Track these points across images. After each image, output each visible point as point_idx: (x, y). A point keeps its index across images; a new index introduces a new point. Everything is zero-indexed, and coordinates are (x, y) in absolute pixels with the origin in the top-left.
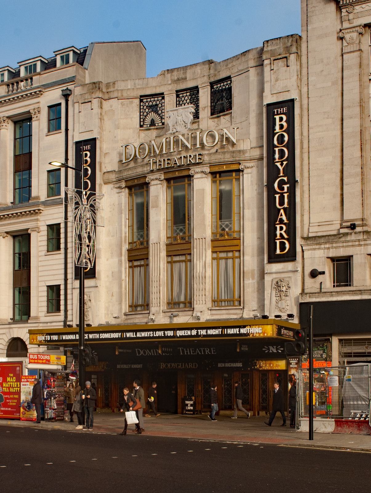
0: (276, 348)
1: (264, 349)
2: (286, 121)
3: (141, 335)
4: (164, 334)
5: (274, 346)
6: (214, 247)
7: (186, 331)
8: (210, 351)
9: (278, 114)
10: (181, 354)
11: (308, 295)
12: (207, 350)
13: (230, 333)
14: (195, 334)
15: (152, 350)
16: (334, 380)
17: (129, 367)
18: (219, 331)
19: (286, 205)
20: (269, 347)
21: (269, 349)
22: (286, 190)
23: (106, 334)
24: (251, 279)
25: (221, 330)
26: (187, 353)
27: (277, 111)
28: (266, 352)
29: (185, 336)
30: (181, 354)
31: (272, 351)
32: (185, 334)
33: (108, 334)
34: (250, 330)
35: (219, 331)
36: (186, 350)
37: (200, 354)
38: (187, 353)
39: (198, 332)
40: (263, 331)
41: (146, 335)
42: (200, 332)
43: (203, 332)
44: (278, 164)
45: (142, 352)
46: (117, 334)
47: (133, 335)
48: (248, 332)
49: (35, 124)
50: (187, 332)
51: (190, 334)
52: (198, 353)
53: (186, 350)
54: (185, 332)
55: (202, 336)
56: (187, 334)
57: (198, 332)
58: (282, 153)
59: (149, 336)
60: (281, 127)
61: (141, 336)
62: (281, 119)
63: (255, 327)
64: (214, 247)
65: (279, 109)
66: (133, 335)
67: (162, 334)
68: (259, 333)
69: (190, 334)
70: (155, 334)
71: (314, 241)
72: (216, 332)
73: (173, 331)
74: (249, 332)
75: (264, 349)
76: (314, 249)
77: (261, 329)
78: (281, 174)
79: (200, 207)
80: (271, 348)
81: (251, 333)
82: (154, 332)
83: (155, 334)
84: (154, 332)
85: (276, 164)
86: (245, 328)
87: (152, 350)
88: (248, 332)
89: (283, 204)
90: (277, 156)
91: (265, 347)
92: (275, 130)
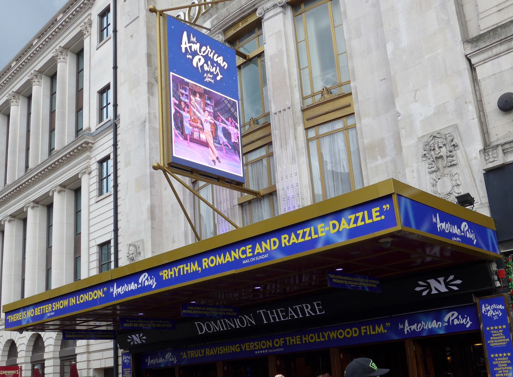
0: (445, 281)
1: (418, 289)
5: (439, 279)
6: (308, 120)
8: (313, 309)
10: (265, 322)
11: (500, 149)
12: (307, 308)
15: (218, 321)
16: (263, 206)
17: (201, 353)
20: (428, 281)
21: (429, 287)
24: (379, 157)
26: (274, 318)
28: (425, 293)
30: (265, 322)
31: (436, 289)
36: (272, 313)
37: (296, 317)
38: (274, 318)
42: (289, 340)
45: (205, 328)
49: (86, 42)
52: (292, 316)
53: (272, 313)
64: (308, 120)
71: (495, 38)
75: (418, 289)
76: (497, 56)
79: (277, 60)
80: (433, 283)
87: (218, 321)
91: (455, 288)
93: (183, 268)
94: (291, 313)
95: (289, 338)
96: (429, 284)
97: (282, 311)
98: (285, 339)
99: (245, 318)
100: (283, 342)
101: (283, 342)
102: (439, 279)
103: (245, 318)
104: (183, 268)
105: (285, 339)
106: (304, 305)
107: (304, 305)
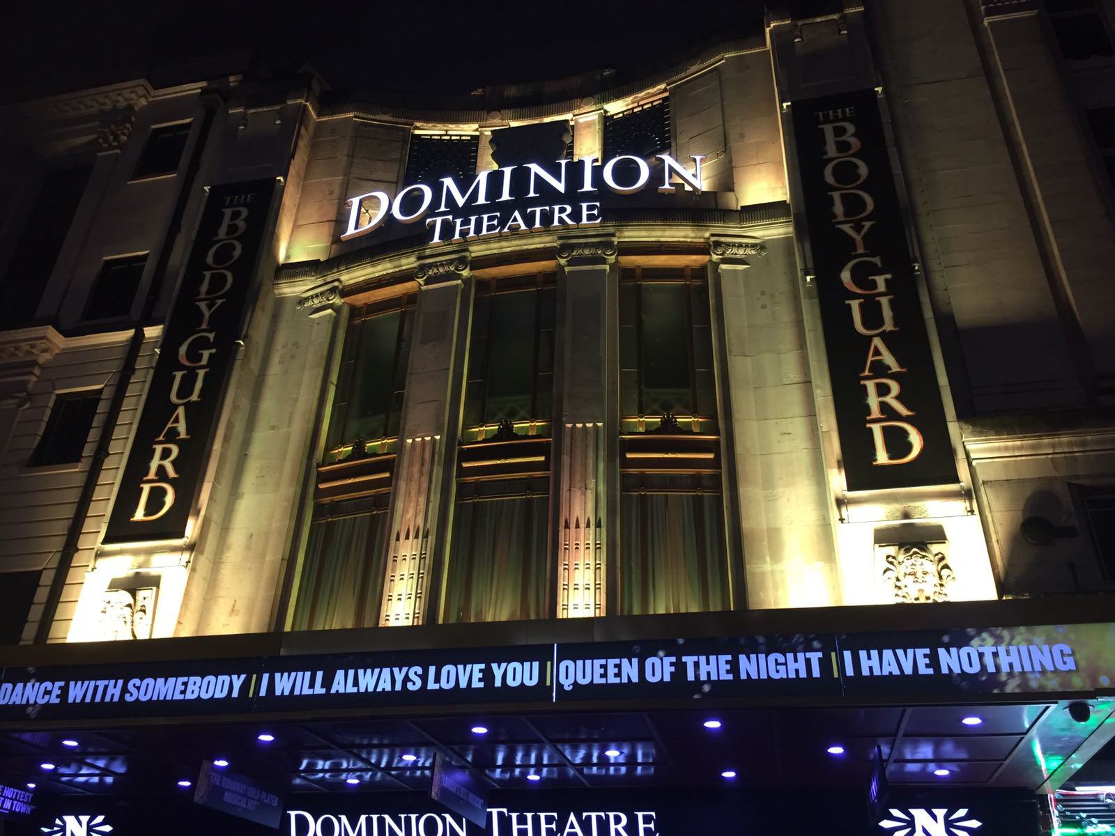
2: (245, 220)
3: (356, 683)
4: (488, 676)
7: (611, 662)
9: (231, 206)
12: (618, 820)
13: (877, 672)
14: (667, 678)
18: (808, 661)
19: (889, 326)
20: (912, 811)
22: (204, 361)
23: (161, 681)
25: (820, 655)
27: (232, 200)
29: (607, 685)
31: (934, 817)
32: (604, 675)
33: (171, 680)
34: (995, 655)
35: (808, 661)
36: (522, 820)
39: (680, 668)
40: (1082, 664)
41: (385, 685)
42: (697, 665)
43: (712, 668)
44: (203, 305)
46: (227, 678)
47: (312, 686)
48: (991, 669)
50: (618, 666)
51: (635, 679)
53: (522, 820)
54: (604, 667)
55: (706, 688)
56: (617, 675)
57: (680, 668)
58: (218, 281)
59: (398, 687)
60: (232, 229)
61: (355, 690)
62: (236, 215)
63: (1030, 642)
65: (236, 197)
66: (312, 686)
67: (477, 675)
68: (1056, 671)
69: (635, 679)
70: (437, 680)
72: (792, 666)
73: (536, 665)
74: (997, 667)
77: (1067, 650)
78: (204, 326)
81: (1011, 674)
82: (432, 669)
83: (437, 680)
84: (432, 669)
85: (197, 303)
86: (967, 644)
88: (991, 669)
89: (881, 323)
90: (204, 288)
92: (216, 235)
93: (106, 687)
94: (572, 826)
95: (695, 658)
96: (912, 817)
97: (549, 820)
98: (679, 659)
99: (444, 820)
100: (673, 669)
101: (673, 669)
102: (935, 811)
103: (444, 820)
104: (106, 687)
105: (679, 659)
106: (611, 815)
107: (611, 815)
